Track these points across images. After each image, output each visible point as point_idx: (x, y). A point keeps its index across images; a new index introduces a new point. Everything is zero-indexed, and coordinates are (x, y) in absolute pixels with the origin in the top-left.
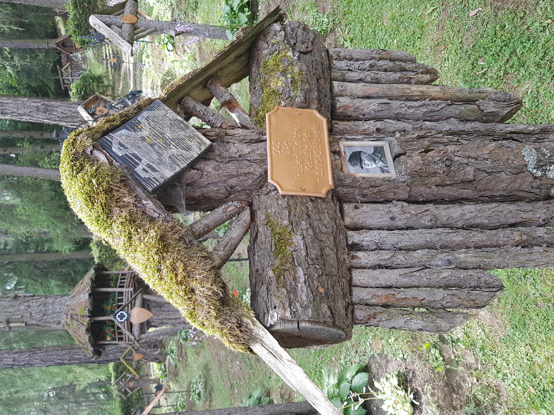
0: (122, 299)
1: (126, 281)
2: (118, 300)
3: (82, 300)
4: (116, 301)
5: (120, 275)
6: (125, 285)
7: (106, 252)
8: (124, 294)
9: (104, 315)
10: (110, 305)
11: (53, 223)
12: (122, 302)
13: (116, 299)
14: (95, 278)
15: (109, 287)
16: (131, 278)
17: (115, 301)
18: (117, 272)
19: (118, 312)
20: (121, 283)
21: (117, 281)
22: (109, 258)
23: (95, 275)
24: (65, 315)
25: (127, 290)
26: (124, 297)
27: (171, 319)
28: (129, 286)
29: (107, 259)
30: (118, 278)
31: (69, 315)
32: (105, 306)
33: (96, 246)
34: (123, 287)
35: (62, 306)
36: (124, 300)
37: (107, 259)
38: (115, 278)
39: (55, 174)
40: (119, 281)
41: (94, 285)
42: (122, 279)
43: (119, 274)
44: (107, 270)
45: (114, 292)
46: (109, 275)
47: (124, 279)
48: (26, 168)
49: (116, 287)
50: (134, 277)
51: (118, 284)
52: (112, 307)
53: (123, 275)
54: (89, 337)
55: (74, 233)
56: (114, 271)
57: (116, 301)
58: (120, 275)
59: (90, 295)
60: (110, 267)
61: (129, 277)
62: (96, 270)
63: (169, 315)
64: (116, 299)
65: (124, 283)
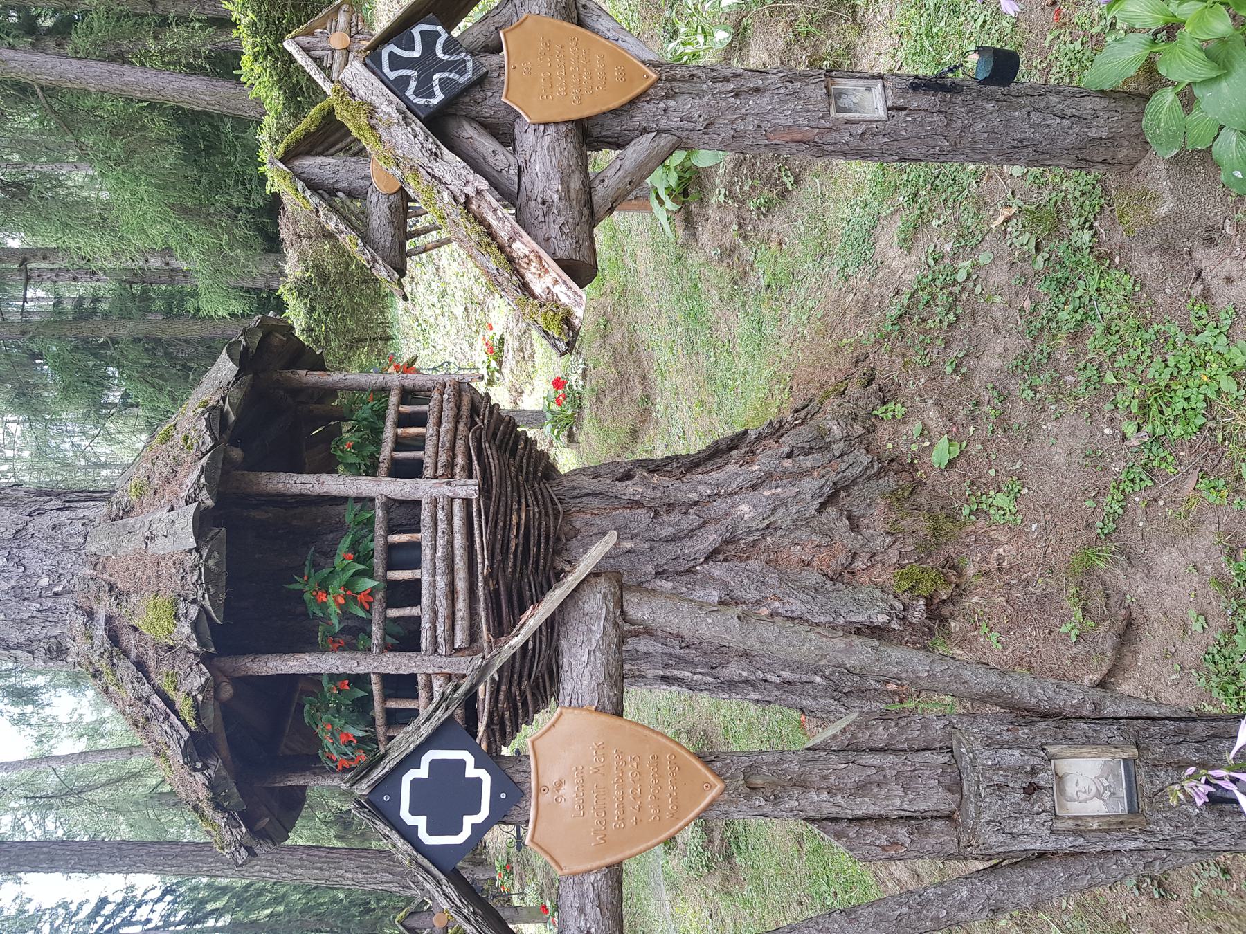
0: (417, 546)
1: (429, 431)
2: (391, 548)
3: (162, 547)
4: (378, 560)
5: (394, 399)
6: (427, 456)
7: (327, 313)
8: (425, 515)
9: (305, 642)
10: (336, 588)
11: (177, 228)
12: (416, 565)
13: (378, 545)
14: (244, 407)
15: (329, 467)
16: (457, 418)
17: (369, 555)
18: (376, 379)
19: (411, 761)
20: (399, 444)
21: (377, 432)
22: (336, 333)
23: (237, 394)
24: (81, 619)
25: (443, 490)
26: (424, 536)
27: (880, 820)
28: (451, 465)
29: (331, 336)
30: (382, 417)
31: (101, 617)
32: (307, 586)
33: (295, 293)
34: (412, 470)
35: (67, 559)
36: (426, 553)
37: (331, 336)
38: (365, 412)
39: (177, 85)
40: (389, 433)
41: (236, 454)
42: (404, 421)
43: (385, 390)
44: (319, 364)
45: (365, 502)
46: (330, 392)
47: (420, 420)
48: (92, 63)
49: (372, 471)
50: (474, 410)
51: (386, 452)
52: (352, 597)
53: (408, 395)
54: (212, 786)
55: (237, 259)
56: (354, 376)
57: (378, 560)
58: (394, 399)
59: (203, 523)
60: (341, 361)
61: (448, 413)
62: (245, 361)
63: (862, 788)
64: (378, 545)
65: (419, 443)
